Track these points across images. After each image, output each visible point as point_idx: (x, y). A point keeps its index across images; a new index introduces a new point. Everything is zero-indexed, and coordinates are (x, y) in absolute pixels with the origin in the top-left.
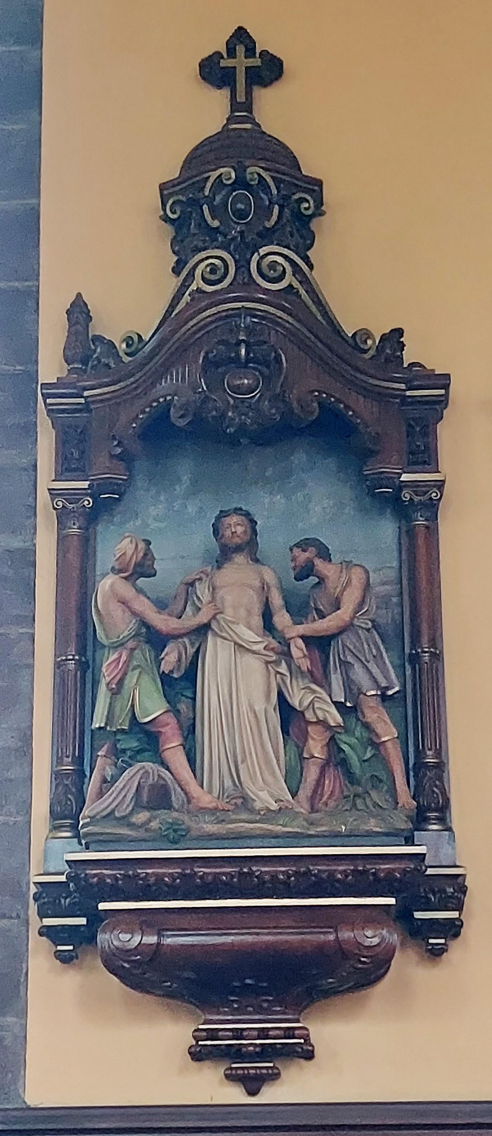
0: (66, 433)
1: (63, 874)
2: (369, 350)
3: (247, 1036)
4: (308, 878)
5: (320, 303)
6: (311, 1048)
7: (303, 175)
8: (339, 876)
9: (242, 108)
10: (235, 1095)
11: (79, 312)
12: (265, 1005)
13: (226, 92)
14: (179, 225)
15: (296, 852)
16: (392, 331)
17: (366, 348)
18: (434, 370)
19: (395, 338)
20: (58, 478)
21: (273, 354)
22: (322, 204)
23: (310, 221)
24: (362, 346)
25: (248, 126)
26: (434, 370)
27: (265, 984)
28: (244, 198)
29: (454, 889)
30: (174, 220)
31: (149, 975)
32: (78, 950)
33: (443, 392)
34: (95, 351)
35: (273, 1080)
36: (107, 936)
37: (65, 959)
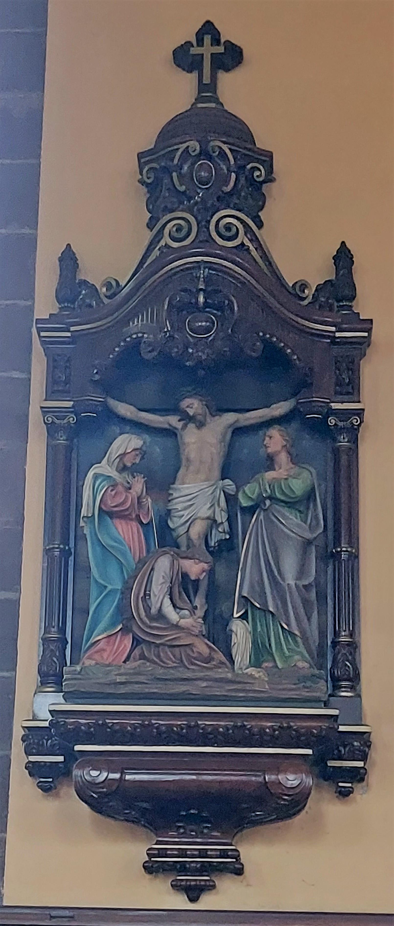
0: (55, 361)
1: (47, 720)
2: (307, 297)
4: (240, 732)
5: (265, 256)
7: (258, 148)
8: (221, 730)
9: (207, 90)
10: (180, 902)
11: (68, 260)
12: (205, 831)
13: (194, 75)
17: (304, 296)
21: (227, 302)
25: (213, 105)
28: (210, 168)
29: (360, 743)
30: (150, 184)
31: (111, 804)
32: (56, 782)
33: (366, 334)
34: (81, 292)
35: (209, 890)
37: (46, 789)
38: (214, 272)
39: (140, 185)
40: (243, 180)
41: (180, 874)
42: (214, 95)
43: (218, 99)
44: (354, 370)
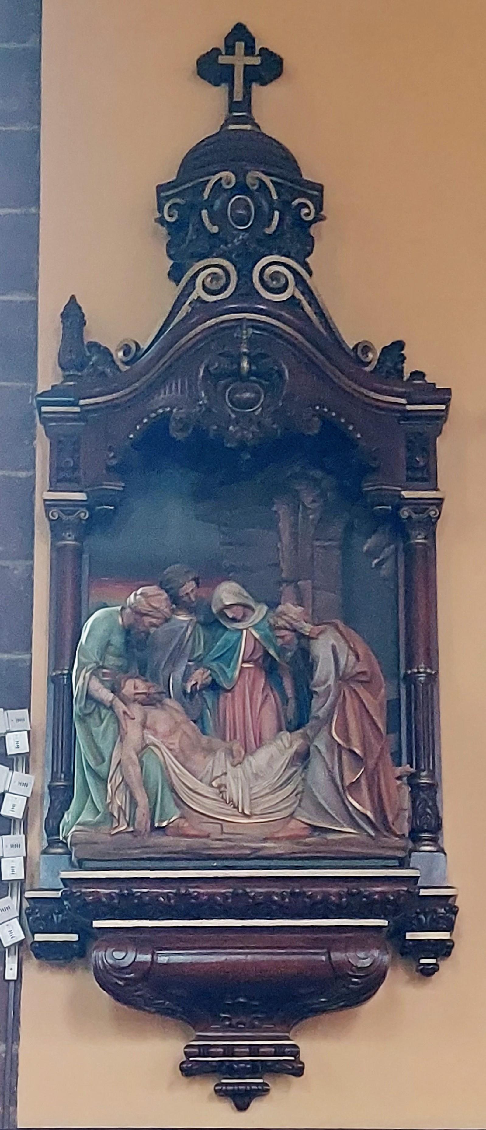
1: (59, 890)
2: (370, 363)
3: (263, 1052)
5: (321, 313)
6: (300, 1065)
9: (240, 108)
11: (73, 315)
13: (224, 88)
14: (176, 230)
15: (86, 875)
16: (393, 343)
17: (368, 360)
18: (434, 384)
19: (396, 350)
20: (52, 489)
22: (321, 209)
23: (310, 227)
24: (362, 358)
25: (248, 127)
26: (434, 384)
27: (257, 1003)
28: (239, 200)
29: (445, 910)
33: (443, 407)
34: (90, 358)
36: (101, 954)
38: (258, 332)
39: (159, 226)
40: (288, 220)
41: (225, 1076)
42: (249, 116)
43: (253, 119)
44: (429, 450)
